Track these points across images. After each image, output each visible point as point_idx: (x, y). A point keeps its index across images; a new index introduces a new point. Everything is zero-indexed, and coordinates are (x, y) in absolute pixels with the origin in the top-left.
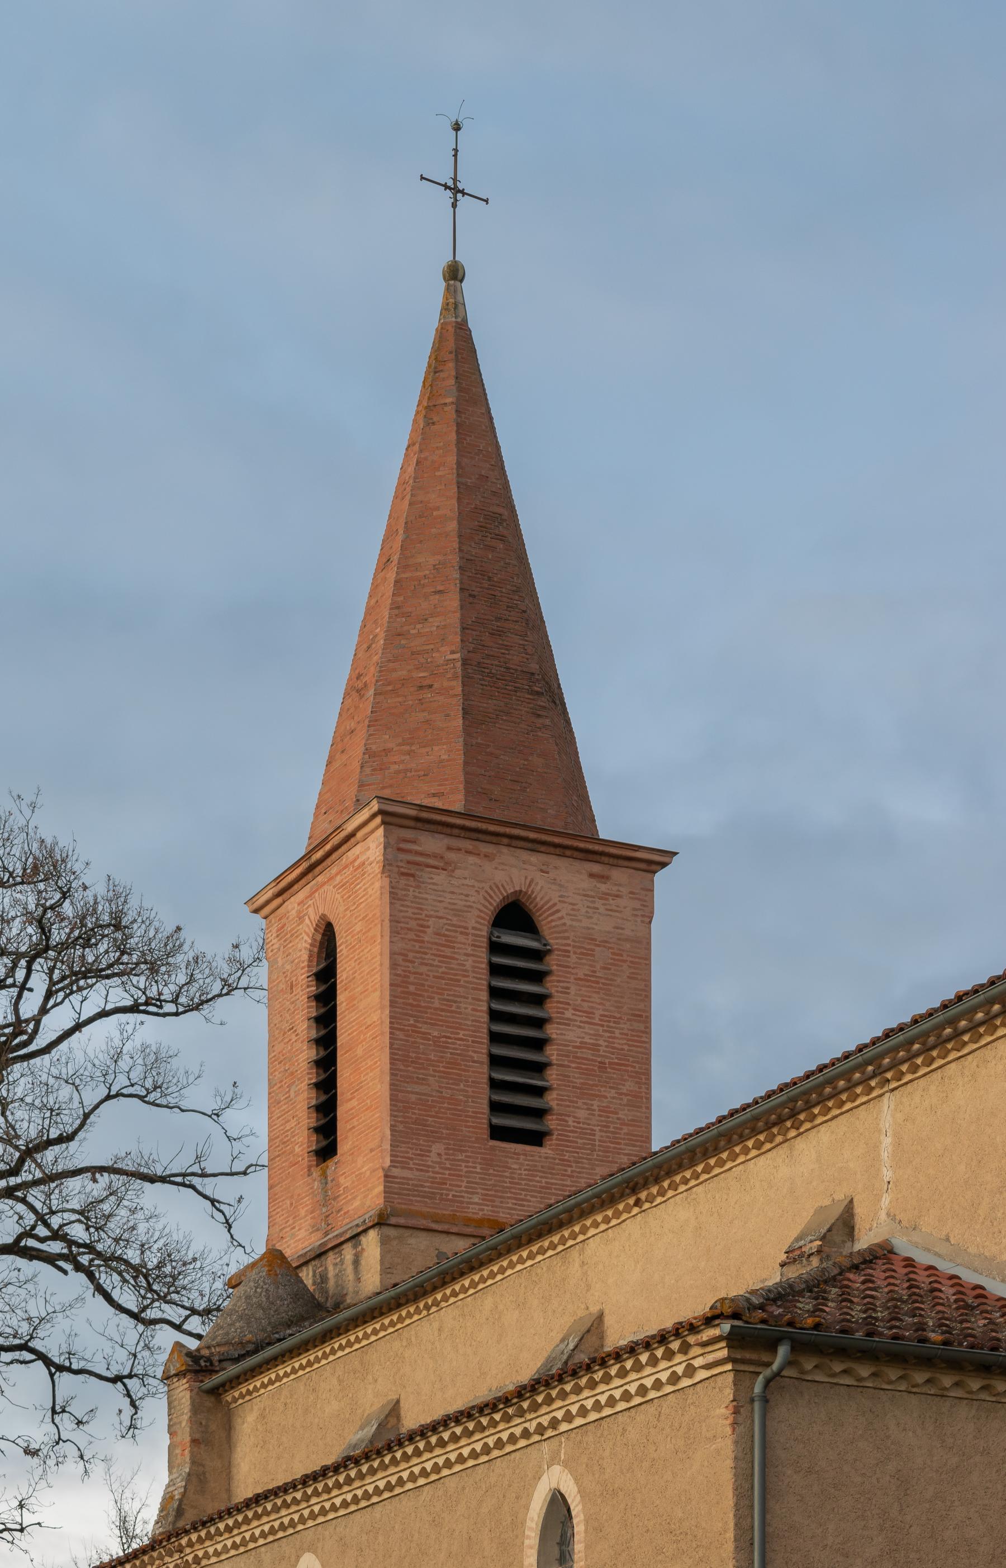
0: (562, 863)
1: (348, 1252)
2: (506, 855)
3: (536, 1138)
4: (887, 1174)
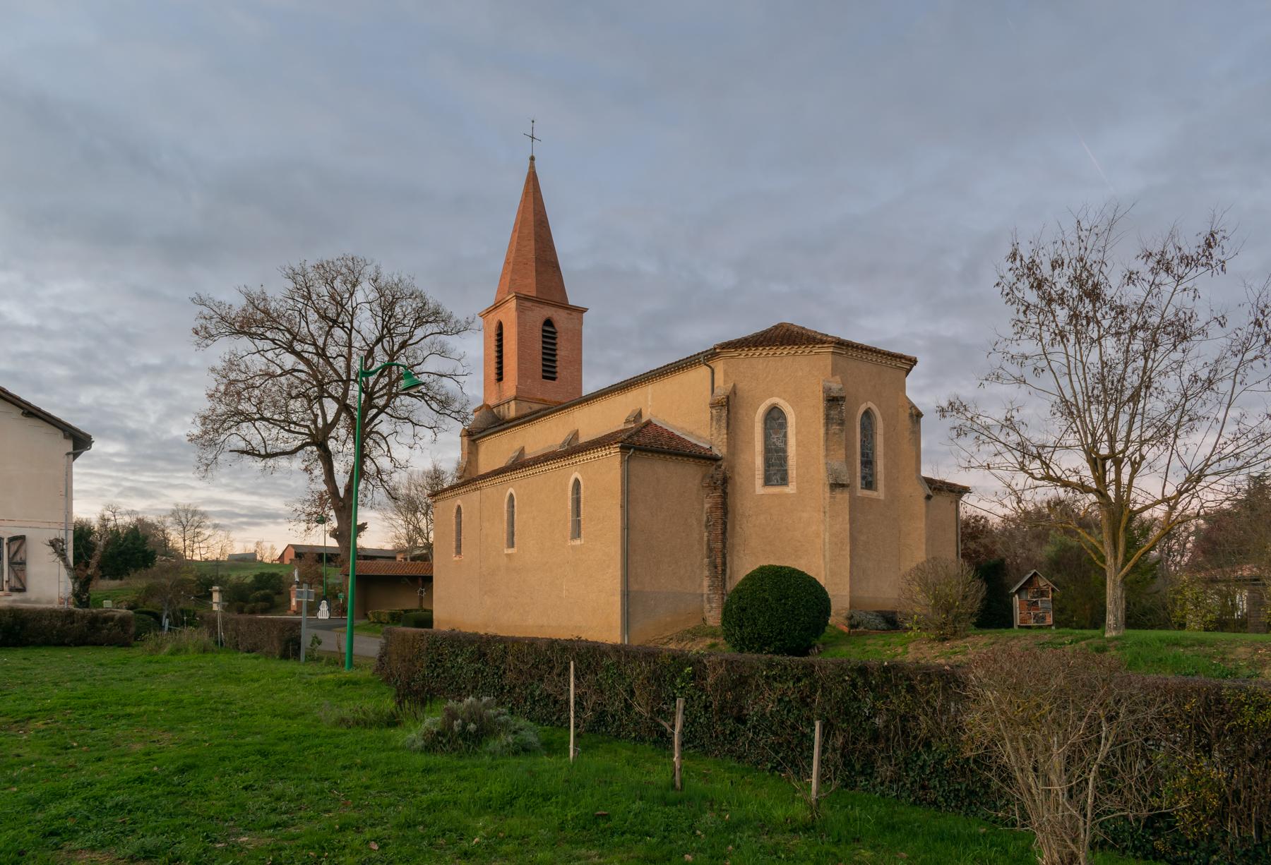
0: (561, 310)
1: (506, 406)
2: (546, 308)
3: (554, 379)
4: (650, 403)
